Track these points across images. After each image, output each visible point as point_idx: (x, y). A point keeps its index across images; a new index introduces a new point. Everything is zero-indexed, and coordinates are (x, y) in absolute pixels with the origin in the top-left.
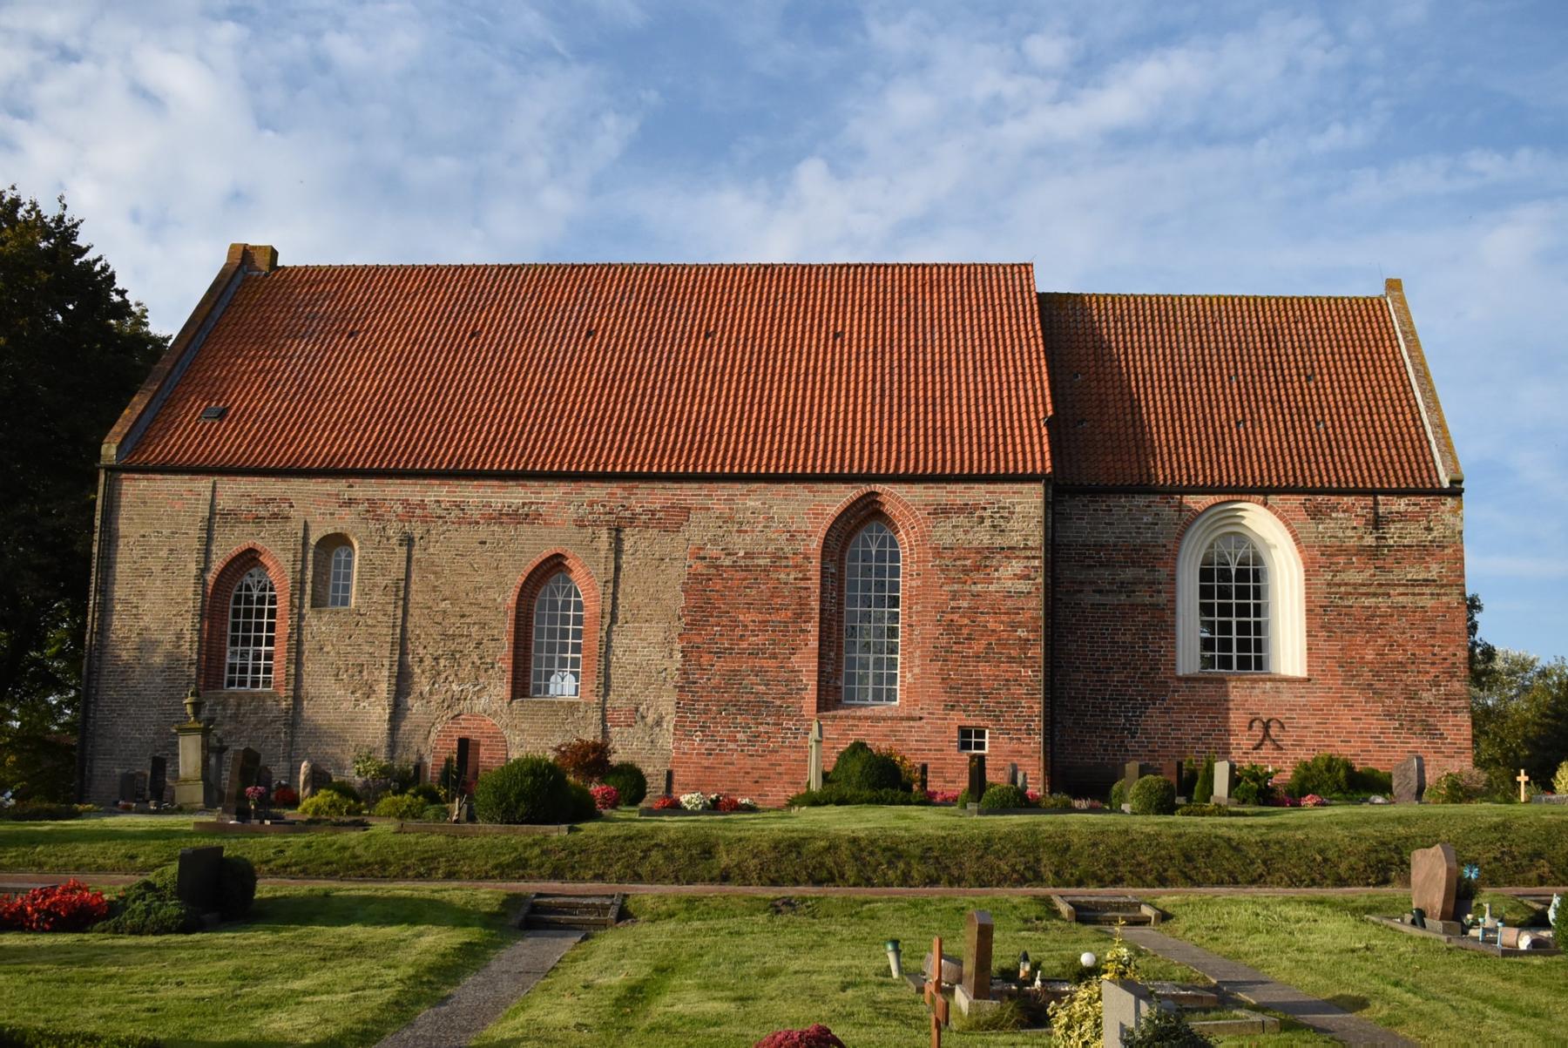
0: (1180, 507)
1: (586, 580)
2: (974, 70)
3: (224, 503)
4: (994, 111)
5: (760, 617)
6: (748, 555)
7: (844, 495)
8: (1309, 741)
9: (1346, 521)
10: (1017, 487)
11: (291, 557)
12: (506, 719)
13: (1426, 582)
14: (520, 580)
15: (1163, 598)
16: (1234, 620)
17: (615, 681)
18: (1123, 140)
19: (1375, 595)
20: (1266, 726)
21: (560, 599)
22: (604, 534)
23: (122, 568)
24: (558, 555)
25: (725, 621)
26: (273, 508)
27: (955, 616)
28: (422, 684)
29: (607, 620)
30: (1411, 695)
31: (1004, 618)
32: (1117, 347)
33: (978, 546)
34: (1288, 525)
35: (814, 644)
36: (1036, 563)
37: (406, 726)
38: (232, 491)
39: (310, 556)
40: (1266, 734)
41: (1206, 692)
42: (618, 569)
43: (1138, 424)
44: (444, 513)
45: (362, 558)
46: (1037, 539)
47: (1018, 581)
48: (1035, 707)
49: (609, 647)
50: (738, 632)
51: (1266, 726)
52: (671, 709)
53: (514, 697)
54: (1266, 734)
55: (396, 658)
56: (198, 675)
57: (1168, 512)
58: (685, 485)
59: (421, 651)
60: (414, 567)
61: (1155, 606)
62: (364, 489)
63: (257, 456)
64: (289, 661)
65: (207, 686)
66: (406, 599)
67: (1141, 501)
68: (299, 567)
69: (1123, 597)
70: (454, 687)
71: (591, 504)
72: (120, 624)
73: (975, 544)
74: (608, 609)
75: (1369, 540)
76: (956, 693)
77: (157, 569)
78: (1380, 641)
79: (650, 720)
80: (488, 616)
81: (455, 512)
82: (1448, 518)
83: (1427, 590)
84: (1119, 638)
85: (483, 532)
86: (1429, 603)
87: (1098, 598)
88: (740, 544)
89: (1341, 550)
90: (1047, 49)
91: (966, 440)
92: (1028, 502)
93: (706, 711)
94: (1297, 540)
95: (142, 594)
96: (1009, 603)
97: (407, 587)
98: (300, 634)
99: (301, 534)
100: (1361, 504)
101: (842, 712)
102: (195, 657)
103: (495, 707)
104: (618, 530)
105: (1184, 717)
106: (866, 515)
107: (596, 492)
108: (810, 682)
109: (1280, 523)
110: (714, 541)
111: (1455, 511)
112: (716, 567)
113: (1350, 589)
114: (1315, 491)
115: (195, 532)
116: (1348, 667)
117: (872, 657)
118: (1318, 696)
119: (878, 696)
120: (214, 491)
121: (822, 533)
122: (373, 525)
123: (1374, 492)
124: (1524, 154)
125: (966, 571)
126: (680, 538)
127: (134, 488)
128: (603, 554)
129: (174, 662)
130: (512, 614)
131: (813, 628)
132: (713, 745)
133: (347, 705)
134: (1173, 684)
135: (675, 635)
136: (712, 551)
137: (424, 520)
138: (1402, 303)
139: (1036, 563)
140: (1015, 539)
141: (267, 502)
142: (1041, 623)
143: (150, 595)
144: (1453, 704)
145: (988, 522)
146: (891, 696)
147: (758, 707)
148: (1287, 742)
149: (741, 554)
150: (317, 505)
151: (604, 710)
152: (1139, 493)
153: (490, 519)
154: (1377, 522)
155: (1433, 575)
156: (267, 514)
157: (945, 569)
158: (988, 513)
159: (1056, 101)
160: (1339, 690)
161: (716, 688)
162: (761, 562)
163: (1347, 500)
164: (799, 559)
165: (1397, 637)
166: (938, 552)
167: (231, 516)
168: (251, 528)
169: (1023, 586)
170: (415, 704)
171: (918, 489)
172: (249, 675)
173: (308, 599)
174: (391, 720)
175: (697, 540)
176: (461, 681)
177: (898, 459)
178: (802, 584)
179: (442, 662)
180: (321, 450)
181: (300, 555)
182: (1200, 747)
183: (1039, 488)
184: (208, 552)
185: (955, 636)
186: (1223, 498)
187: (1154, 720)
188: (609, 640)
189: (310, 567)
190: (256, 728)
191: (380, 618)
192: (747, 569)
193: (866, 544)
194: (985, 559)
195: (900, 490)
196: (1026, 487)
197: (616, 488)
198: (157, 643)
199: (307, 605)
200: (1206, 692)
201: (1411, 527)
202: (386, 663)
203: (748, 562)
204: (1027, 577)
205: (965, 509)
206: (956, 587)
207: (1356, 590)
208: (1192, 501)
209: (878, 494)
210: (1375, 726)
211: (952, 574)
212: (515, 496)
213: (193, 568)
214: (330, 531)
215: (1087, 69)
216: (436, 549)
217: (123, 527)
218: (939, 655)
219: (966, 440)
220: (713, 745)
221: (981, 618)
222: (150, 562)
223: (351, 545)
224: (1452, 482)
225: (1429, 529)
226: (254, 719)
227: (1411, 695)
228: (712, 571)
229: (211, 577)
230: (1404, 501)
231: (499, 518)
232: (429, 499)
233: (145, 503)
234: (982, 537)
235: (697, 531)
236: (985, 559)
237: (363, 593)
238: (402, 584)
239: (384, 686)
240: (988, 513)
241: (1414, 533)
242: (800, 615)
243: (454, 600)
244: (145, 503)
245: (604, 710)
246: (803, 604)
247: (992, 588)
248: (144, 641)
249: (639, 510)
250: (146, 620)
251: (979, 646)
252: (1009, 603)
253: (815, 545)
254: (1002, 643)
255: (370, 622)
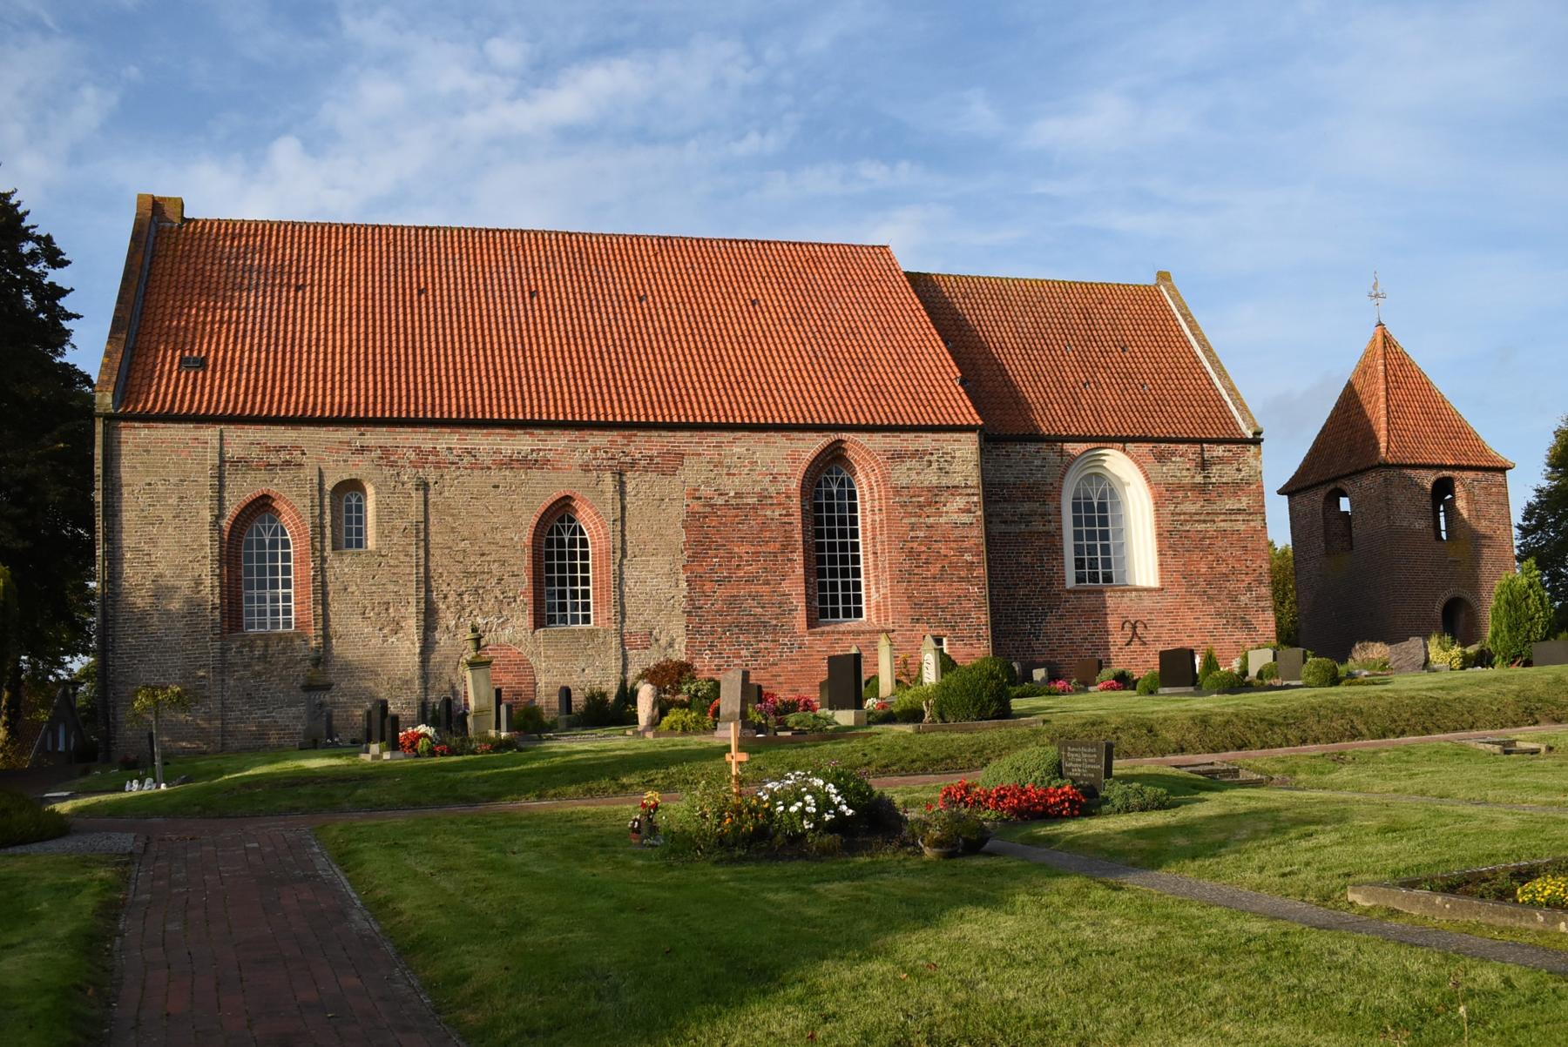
0: (1062, 453)
1: (593, 524)
2: (444, 68)
3: (232, 451)
4: (458, 104)
5: (753, 549)
6: (738, 495)
8: (1165, 637)
9: (1181, 466)
10: (956, 435)
11: (308, 502)
12: (530, 648)
13: (1239, 511)
14: (534, 520)
15: (1052, 527)
17: (629, 610)
18: (572, 136)
19: (1205, 522)
20: (1134, 627)
22: (608, 477)
23: (129, 516)
24: (567, 497)
25: (722, 552)
26: (284, 456)
27: (915, 545)
28: (447, 618)
29: (619, 555)
31: (953, 545)
32: (972, 320)
33: (920, 489)
34: (1141, 467)
35: (800, 571)
36: (975, 499)
37: (436, 658)
38: (240, 440)
39: (327, 500)
40: (1135, 634)
41: (1088, 602)
42: (623, 508)
43: (1009, 383)
45: (378, 503)
46: (974, 479)
47: (961, 513)
48: (983, 617)
49: (622, 579)
50: (735, 562)
51: (1134, 627)
52: (682, 631)
53: (536, 628)
54: (1135, 634)
55: (422, 595)
56: (222, 618)
57: (1053, 457)
58: (679, 434)
59: (444, 588)
60: (431, 510)
61: (1047, 533)
62: (377, 437)
63: (260, 406)
64: (316, 602)
65: (231, 630)
66: (426, 540)
67: (1032, 447)
68: (317, 512)
70: (479, 620)
71: (595, 450)
72: (133, 573)
73: (926, 483)
74: (619, 545)
75: (1199, 479)
77: (167, 516)
78: (1210, 558)
79: (663, 642)
80: (506, 554)
81: (467, 459)
82: (1252, 461)
83: (1240, 517)
84: (1023, 560)
85: (496, 476)
86: (1241, 526)
88: (731, 486)
89: (1181, 487)
90: (507, 52)
91: (453, 387)
92: (966, 448)
93: (713, 632)
94: (1147, 478)
95: (153, 541)
96: (957, 532)
97: (426, 528)
98: (324, 576)
99: (316, 481)
101: (827, 629)
102: (217, 601)
103: (519, 636)
104: (621, 474)
106: (832, 462)
107: (599, 439)
108: (799, 603)
109: (1135, 467)
110: (707, 483)
111: (1257, 456)
112: (711, 506)
114: (1159, 440)
115: (206, 480)
118: (1168, 602)
119: (847, 614)
120: (221, 439)
121: (800, 475)
122: (387, 471)
123: (1201, 441)
124: (904, 166)
125: (920, 507)
126: (677, 480)
127: (133, 437)
128: (609, 495)
129: (194, 608)
130: (528, 552)
131: (798, 557)
132: (722, 661)
133: (376, 642)
134: (1064, 596)
135: (680, 567)
136: (705, 491)
137: (437, 465)
138: (1172, 289)
139: (975, 499)
140: (958, 480)
141: (278, 449)
142: (983, 548)
143: (162, 542)
144: (1262, 604)
145: (935, 466)
146: (859, 613)
147: (759, 626)
148: (1149, 638)
150: (328, 454)
151: (622, 635)
152: (1031, 441)
153: (501, 465)
154: (1204, 465)
155: (1243, 505)
156: (279, 462)
157: (904, 505)
159: (512, 98)
160: (1184, 597)
161: (720, 612)
162: (750, 501)
164: (782, 498)
165: (1222, 554)
166: (897, 491)
167: (242, 463)
168: (263, 475)
169: (966, 518)
170: (441, 637)
171: (878, 437)
173: (328, 542)
174: (421, 653)
175: (692, 483)
176: (486, 615)
177: (227, 401)
178: (786, 519)
179: (466, 597)
181: (317, 501)
183: (974, 436)
184: (221, 499)
185: (915, 562)
186: (1093, 445)
187: (1052, 625)
188: (621, 573)
189: (328, 511)
190: (285, 667)
191: (402, 558)
192: (737, 507)
194: (936, 495)
195: (862, 438)
196: (963, 436)
198: (175, 589)
199: (328, 548)
200: (1088, 602)
201: (1227, 469)
202: (413, 600)
203: (738, 501)
204: (969, 511)
205: (916, 454)
206: (913, 520)
207: (1192, 517)
208: (1068, 447)
209: (842, 441)
210: (1210, 623)
211: (910, 509)
212: (523, 443)
213: (207, 516)
214: (346, 477)
215: (542, 71)
216: (452, 491)
217: (125, 475)
218: (903, 577)
219: (453, 387)
220: (722, 661)
221: (935, 546)
222: (159, 510)
223: (363, 491)
225: (1239, 470)
226: (283, 659)
228: (708, 509)
229: (225, 523)
230: (1221, 448)
231: (509, 463)
232: (441, 446)
233: (148, 451)
234: (931, 478)
235: (692, 474)
236: (936, 495)
237: (381, 535)
238: (422, 526)
239: (412, 622)
241: (1228, 473)
242: (786, 547)
243: (473, 540)
244: (148, 451)
245: (622, 635)
246: (788, 537)
247: (942, 520)
248: (159, 587)
249: (638, 456)
250: (161, 567)
251: (935, 569)
252: (957, 532)
253: (795, 485)
254: (953, 566)
255: (392, 562)
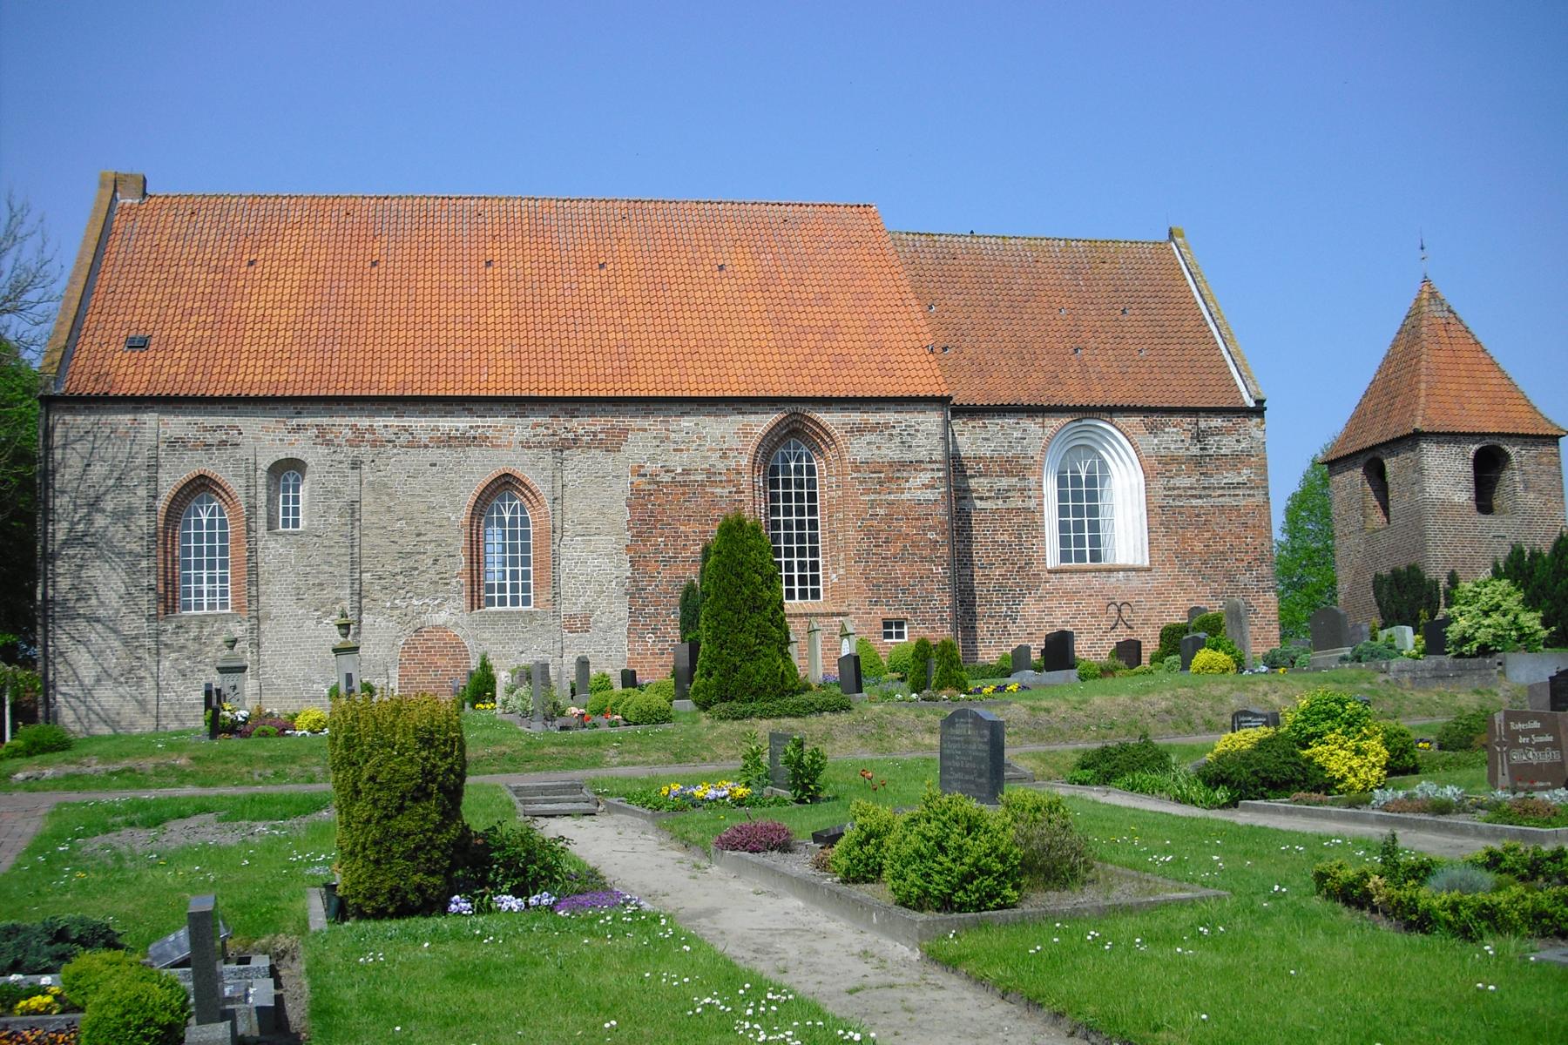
6: (686, 472)
7: (763, 422)
13: (1239, 485)
15: (1032, 504)
16: (796, 560)
19: (1200, 497)
21: (507, 516)
27: (875, 523)
30: (1231, 578)
36: (941, 474)
44: (393, 437)
69: (1000, 502)
75: (1195, 450)
76: (879, 590)
78: (1207, 535)
85: (433, 454)
100: (1187, 422)
105: (1054, 603)
110: (652, 459)
112: (657, 483)
113: (1181, 492)
116: (1182, 557)
121: (751, 450)
136: (649, 468)
137: (374, 444)
139: (941, 474)
140: (922, 454)
149: (679, 470)
154: (1199, 436)
162: (699, 478)
168: (200, 454)
169: (930, 495)
178: (736, 497)
180: (254, 378)
185: (879, 535)
203: (686, 478)
204: (933, 487)
206: (873, 497)
212: (460, 423)
224: (1257, 402)
227: (1231, 578)
231: (448, 441)
234: (891, 452)
240: (896, 432)
241: (1228, 445)
249: (581, 432)
251: (893, 549)
253: (745, 461)
255: (327, 543)
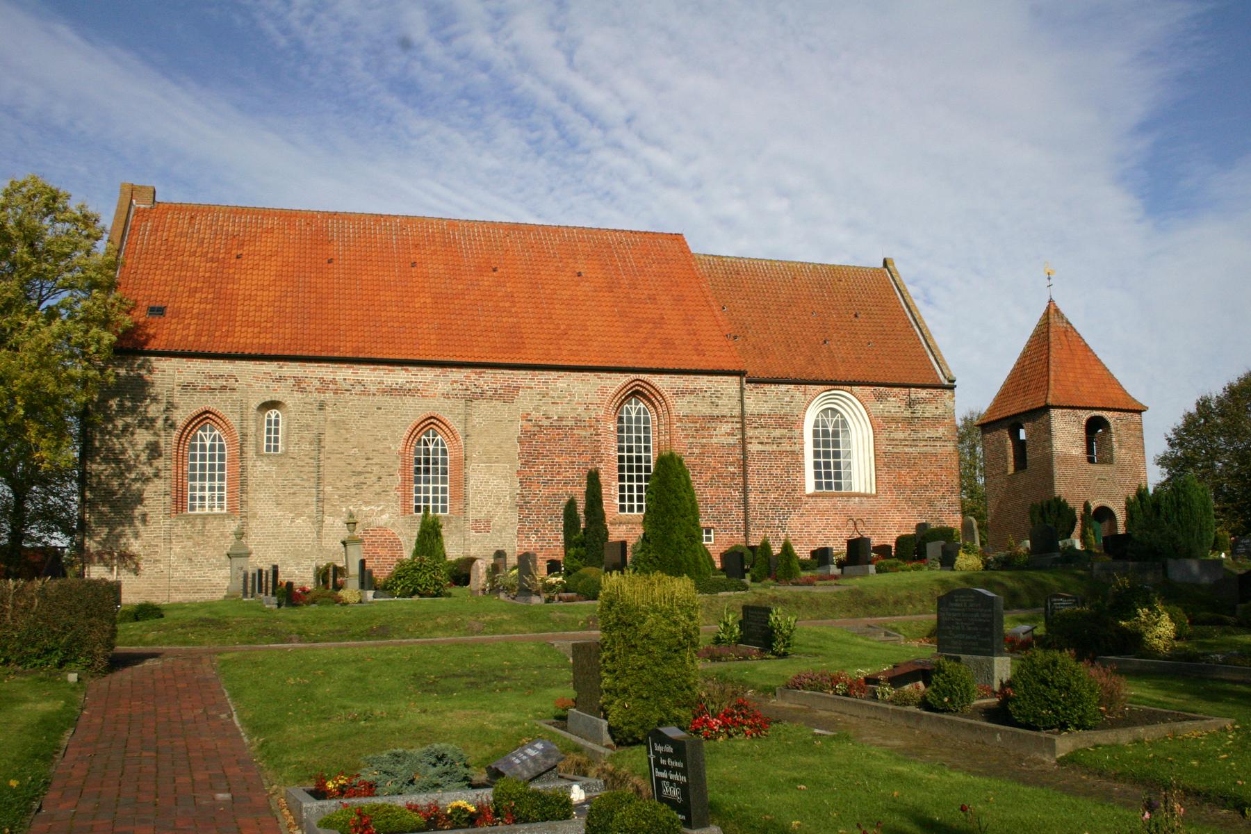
9: (894, 403)
15: (797, 448)
26: (222, 382)
61: (793, 452)
62: (292, 370)
63: (205, 344)
75: (907, 414)
84: (774, 472)
87: (760, 447)
89: (894, 420)
112: (540, 426)
117: (431, 486)
134: (804, 499)
136: (534, 415)
140: (726, 411)
153: (384, 392)
154: (910, 404)
158: (708, 394)
163: (896, 390)
168: (207, 395)
171: (666, 377)
172: (635, 494)
182: (821, 537)
193: (628, 412)
196: (730, 379)
197: (507, 373)
204: (733, 435)
212: (399, 376)
231: (391, 391)
234: (704, 409)
240: (708, 394)
241: (930, 411)
247: (714, 440)
255: (300, 463)
